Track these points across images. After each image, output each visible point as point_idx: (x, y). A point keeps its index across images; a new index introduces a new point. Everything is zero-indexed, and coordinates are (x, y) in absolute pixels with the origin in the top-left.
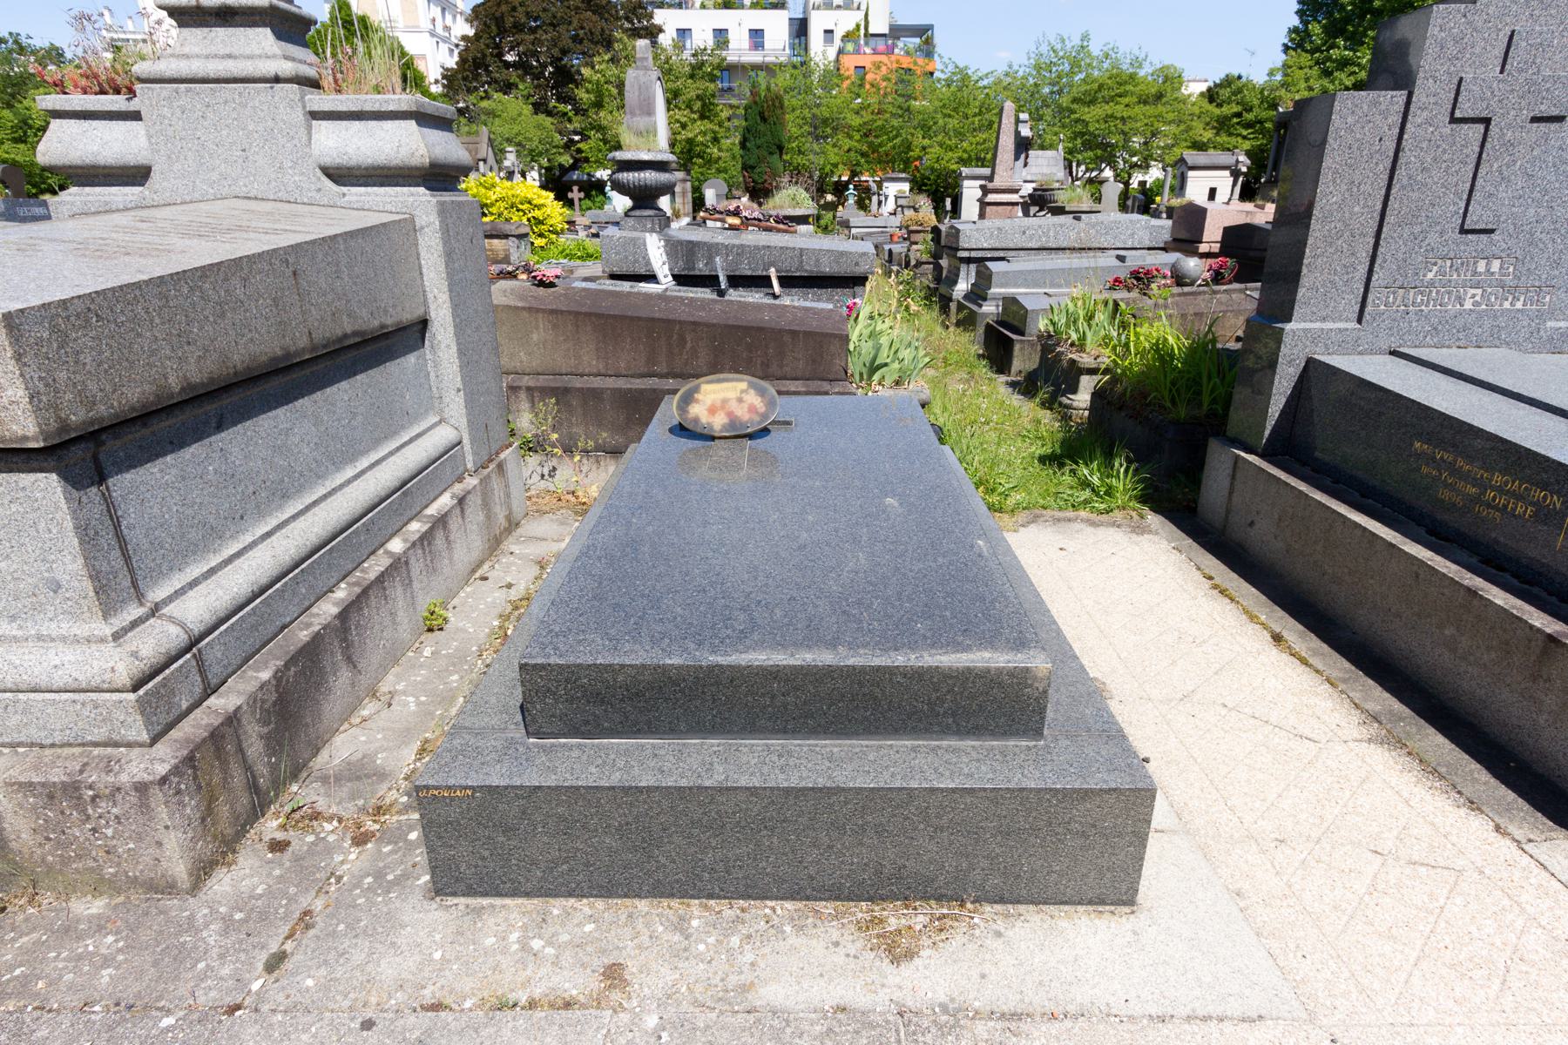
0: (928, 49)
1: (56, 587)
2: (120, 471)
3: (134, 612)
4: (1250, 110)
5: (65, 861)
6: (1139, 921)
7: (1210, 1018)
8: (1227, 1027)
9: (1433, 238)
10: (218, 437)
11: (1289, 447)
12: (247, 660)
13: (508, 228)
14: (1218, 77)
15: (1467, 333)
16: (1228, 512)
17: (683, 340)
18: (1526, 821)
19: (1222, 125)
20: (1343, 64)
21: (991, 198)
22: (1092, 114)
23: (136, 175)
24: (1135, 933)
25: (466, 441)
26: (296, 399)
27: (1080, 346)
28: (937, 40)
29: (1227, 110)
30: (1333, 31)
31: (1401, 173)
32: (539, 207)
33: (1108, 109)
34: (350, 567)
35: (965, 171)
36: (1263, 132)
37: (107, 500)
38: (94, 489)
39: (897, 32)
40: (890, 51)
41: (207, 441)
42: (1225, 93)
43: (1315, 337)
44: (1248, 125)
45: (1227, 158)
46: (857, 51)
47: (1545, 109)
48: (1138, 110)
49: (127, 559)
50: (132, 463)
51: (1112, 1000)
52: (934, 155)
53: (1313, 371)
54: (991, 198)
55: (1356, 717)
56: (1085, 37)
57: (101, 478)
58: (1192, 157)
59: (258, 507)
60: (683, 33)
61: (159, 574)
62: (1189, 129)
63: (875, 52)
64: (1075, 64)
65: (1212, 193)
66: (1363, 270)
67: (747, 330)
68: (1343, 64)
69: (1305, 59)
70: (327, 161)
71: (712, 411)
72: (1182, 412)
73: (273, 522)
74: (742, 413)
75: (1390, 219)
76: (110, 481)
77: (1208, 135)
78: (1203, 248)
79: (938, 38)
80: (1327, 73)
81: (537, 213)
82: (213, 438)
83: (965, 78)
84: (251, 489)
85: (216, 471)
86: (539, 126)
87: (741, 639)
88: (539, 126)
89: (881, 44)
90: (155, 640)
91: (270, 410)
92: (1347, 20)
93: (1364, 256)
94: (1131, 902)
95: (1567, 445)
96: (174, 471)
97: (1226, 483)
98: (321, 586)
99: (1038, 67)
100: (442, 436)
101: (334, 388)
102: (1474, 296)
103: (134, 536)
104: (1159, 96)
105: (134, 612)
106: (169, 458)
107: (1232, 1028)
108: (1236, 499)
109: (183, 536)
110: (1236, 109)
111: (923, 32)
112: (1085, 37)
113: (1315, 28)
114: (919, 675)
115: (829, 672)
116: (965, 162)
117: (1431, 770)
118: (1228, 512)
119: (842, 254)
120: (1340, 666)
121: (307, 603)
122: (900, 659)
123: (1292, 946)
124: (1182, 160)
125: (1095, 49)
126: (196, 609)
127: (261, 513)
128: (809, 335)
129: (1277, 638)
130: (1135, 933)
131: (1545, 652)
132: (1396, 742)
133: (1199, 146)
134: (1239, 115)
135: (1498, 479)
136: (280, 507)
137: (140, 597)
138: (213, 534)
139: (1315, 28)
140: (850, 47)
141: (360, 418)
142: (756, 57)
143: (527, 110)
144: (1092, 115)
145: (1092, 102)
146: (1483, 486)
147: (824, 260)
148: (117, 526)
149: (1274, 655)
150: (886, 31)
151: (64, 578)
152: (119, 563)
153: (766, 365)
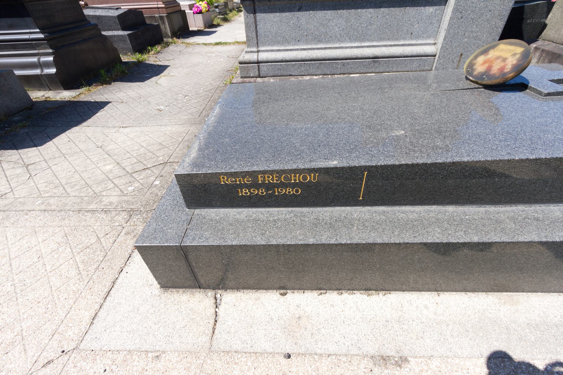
2: (261, 12)
3: (255, 49)
7: (104, 302)
8: (97, 306)
10: (298, 13)
12: (274, 76)
24: (151, 285)
25: (437, 56)
26: (340, 9)
34: (329, 73)
37: (255, 18)
38: (252, 15)
41: (293, 13)
49: (257, 37)
50: (265, 11)
51: (130, 268)
57: (255, 13)
59: (306, 40)
61: (265, 44)
73: (309, 47)
76: (257, 14)
82: (296, 13)
84: (306, 34)
85: (293, 23)
90: (253, 57)
91: (324, 10)
96: (278, 18)
98: (311, 71)
100: (429, 50)
101: (364, 10)
102: (426, 307)
103: (260, 31)
105: (255, 49)
106: (277, 14)
107: (96, 308)
109: (276, 37)
121: (303, 73)
123: (114, 367)
126: (263, 56)
127: (307, 42)
130: (151, 285)
136: (316, 44)
137: (258, 47)
138: (286, 41)
141: (375, 27)
148: (256, 27)
152: (255, 36)
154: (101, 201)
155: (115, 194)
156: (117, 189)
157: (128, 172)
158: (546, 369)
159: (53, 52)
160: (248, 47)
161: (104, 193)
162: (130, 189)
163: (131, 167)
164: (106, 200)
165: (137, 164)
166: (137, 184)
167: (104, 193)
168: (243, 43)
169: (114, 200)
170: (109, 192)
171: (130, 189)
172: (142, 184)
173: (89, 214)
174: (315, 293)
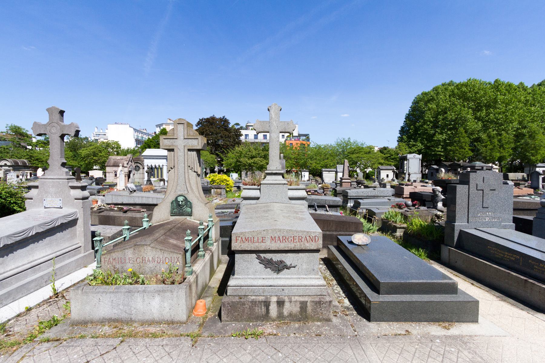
0: (308, 139)
1: (314, 270)
3: (156, 170)
4: (392, 155)
5: (314, 315)
6: (479, 325)
9: (478, 209)
11: (460, 246)
13: (222, 187)
14: (382, 147)
15: (487, 225)
16: (449, 259)
17: (330, 224)
18: (532, 312)
19: (386, 159)
20: (414, 145)
21: (343, 181)
22: (354, 156)
23: (258, 198)
27: (396, 222)
28: (310, 137)
29: (386, 155)
30: (409, 138)
31: (470, 198)
32: (228, 181)
33: (357, 155)
35: (323, 169)
36: (396, 160)
39: (300, 135)
40: (299, 140)
42: (385, 151)
43: (461, 226)
44: (393, 159)
45: (389, 167)
46: (291, 140)
47: (492, 188)
48: (365, 155)
52: (313, 165)
53: (461, 232)
54: (343, 181)
55: (495, 297)
56: (349, 138)
58: (380, 166)
60: (247, 135)
62: (378, 160)
63: (295, 140)
64: (347, 145)
65: (387, 176)
66: (467, 214)
67: (343, 222)
68: (414, 145)
69: (404, 144)
70: (290, 196)
71: (358, 240)
72: (431, 238)
74: (364, 240)
75: (470, 206)
77: (382, 161)
78: (404, 196)
79: (311, 137)
80: (410, 148)
81: (228, 183)
83: (320, 147)
86: (212, 157)
87: (408, 278)
88: (212, 157)
89: (296, 138)
92: (412, 135)
93: (466, 211)
94: (477, 322)
95: (544, 257)
97: (448, 254)
99: (337, 145)
104: (369, 152)
108: (451, 257)
110: (389, 155)
111: (306, 135)
112: (349, 138)
113: (405, 137)
114: (439, 284)
115: (426, 283)
116: (322, 167)
117: (513, 305)
118: (449, 259)
119: (335, 201)
120: (487, 289)
122: (435, 281)
124: (379, 168)
125: (352, 141)
128: (355, 223)
129: (472, 284)
131: (525, 283)
132: (505, 301)
133: (382, 164)
134: (390, 157)
135: (506, 253)
139: (405, 137)
140: (289, 139)
142: (265, 141)
143: (208, 153)
144: (354, 156)
145: (353, 154)
146: (504, 255)
147: (331, 202)
149: (473, 287)
150: (297, 135)
151: (315, 269)
153: (347, 229)
154: (473, 358)
155: (462, 354)
156: (459, 356)
157: (443, 358)
158: (233, 251)
159: (443, 199)
160: (281, 262)
161: (468, 360)
162: (453, 350)
163: (438, 358)
164: (470, 356)
165: (433, 356)
166: (447, 348)
167: (468, 360)
168: (27, 199)
169: (466, 352)
170: (465, 358)
171: (453, 350)
172: (445, 346)
173: (484, 358)
174: (33, 245)
